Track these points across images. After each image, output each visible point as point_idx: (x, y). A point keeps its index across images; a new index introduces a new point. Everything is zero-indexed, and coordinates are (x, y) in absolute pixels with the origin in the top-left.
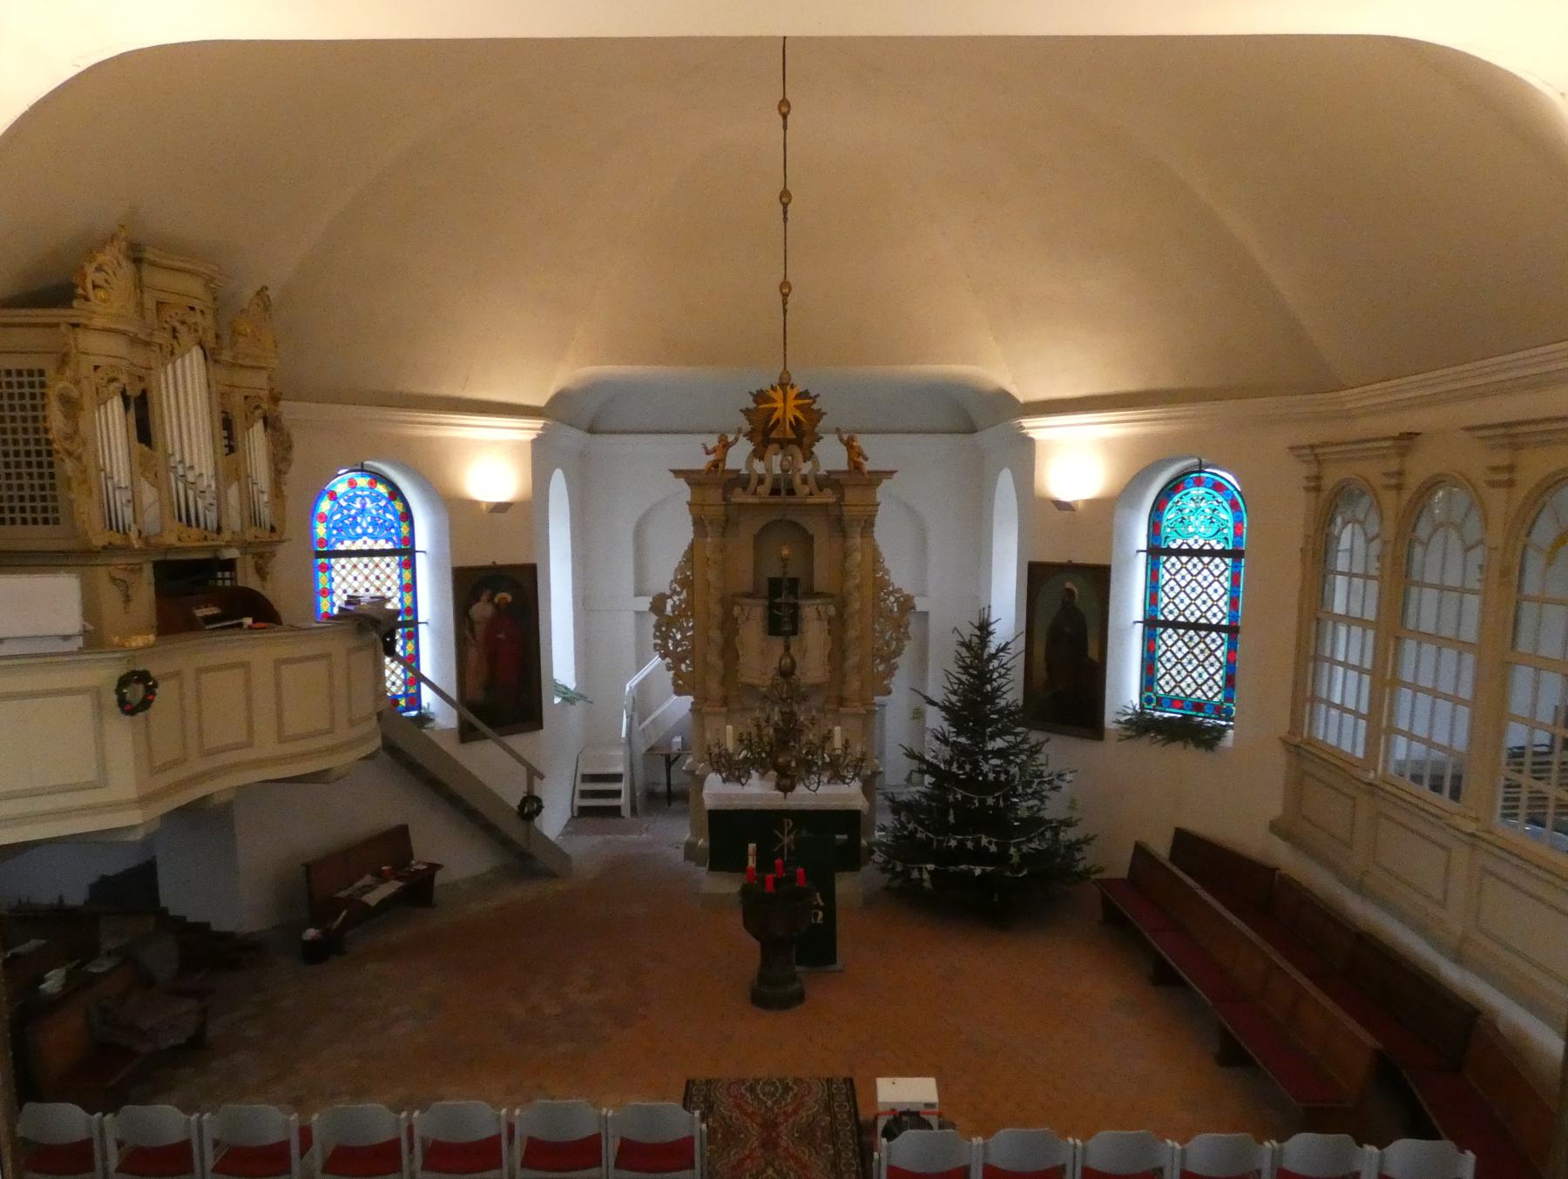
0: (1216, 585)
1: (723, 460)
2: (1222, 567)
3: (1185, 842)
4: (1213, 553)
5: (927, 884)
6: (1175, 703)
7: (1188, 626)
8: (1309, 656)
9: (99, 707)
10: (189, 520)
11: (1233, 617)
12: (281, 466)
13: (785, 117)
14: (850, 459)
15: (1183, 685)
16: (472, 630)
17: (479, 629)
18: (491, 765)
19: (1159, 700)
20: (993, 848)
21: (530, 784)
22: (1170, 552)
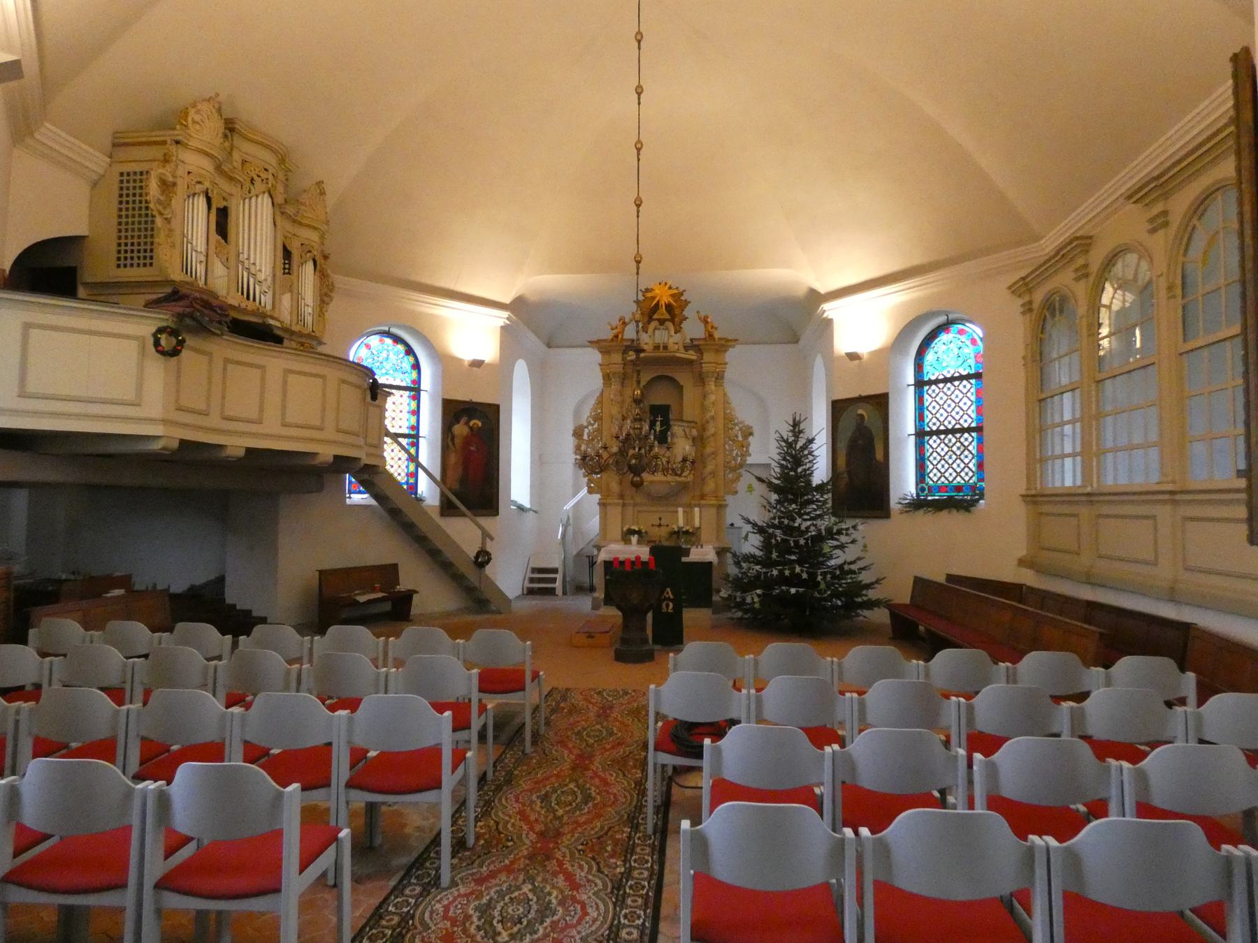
0: (965, 399)
1: (622, 332)
2: (969, 386)
3: (950, 578)
4: (961, 378)
5: (757, 606)
6: (942, 488)
7: (947, 432)
8: (1038, 430)
9: (143, 348)
10: (248, 298)
11: (980, 421)
12: (326, 299)
13: (639, 42)
14: (706, 330)
15: (947, 475)
16: (453, 440)
17: (458, 441)
18: (463, 533)
19: (930, 488)
20: (805, 576)
21: (484, 543)
22: (930, 383)
